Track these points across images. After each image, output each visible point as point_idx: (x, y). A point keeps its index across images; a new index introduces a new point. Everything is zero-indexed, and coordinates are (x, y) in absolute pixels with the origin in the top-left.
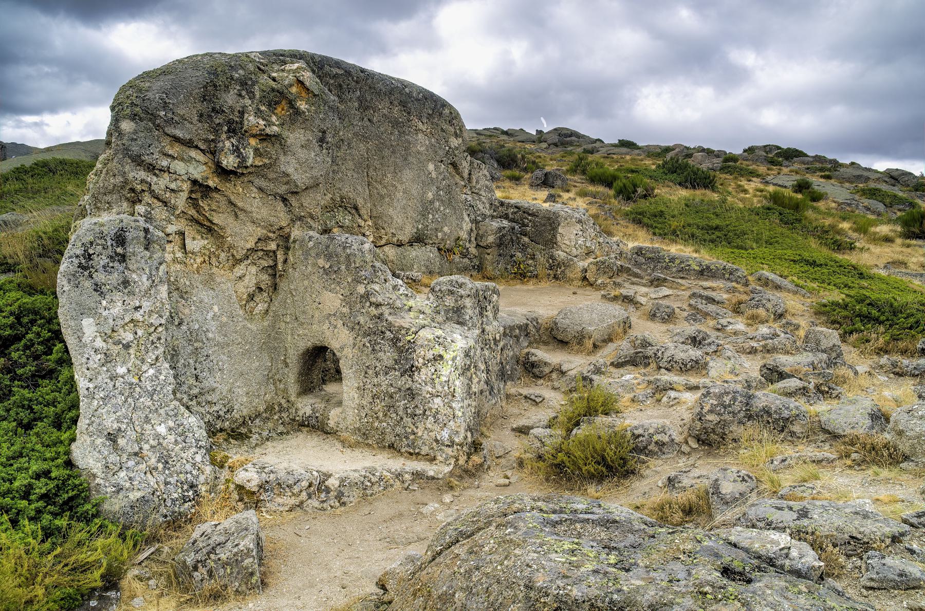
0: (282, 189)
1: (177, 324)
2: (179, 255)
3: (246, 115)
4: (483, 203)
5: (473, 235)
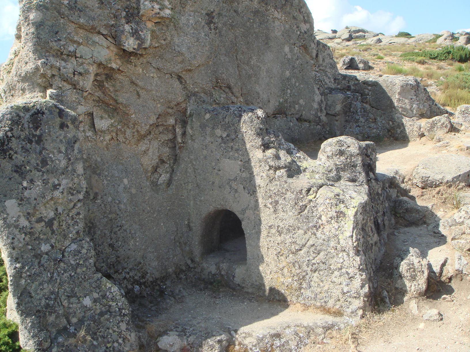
0: (177, 68)
1: (92, 198)
2: (90, 134)
4: (329, 78)
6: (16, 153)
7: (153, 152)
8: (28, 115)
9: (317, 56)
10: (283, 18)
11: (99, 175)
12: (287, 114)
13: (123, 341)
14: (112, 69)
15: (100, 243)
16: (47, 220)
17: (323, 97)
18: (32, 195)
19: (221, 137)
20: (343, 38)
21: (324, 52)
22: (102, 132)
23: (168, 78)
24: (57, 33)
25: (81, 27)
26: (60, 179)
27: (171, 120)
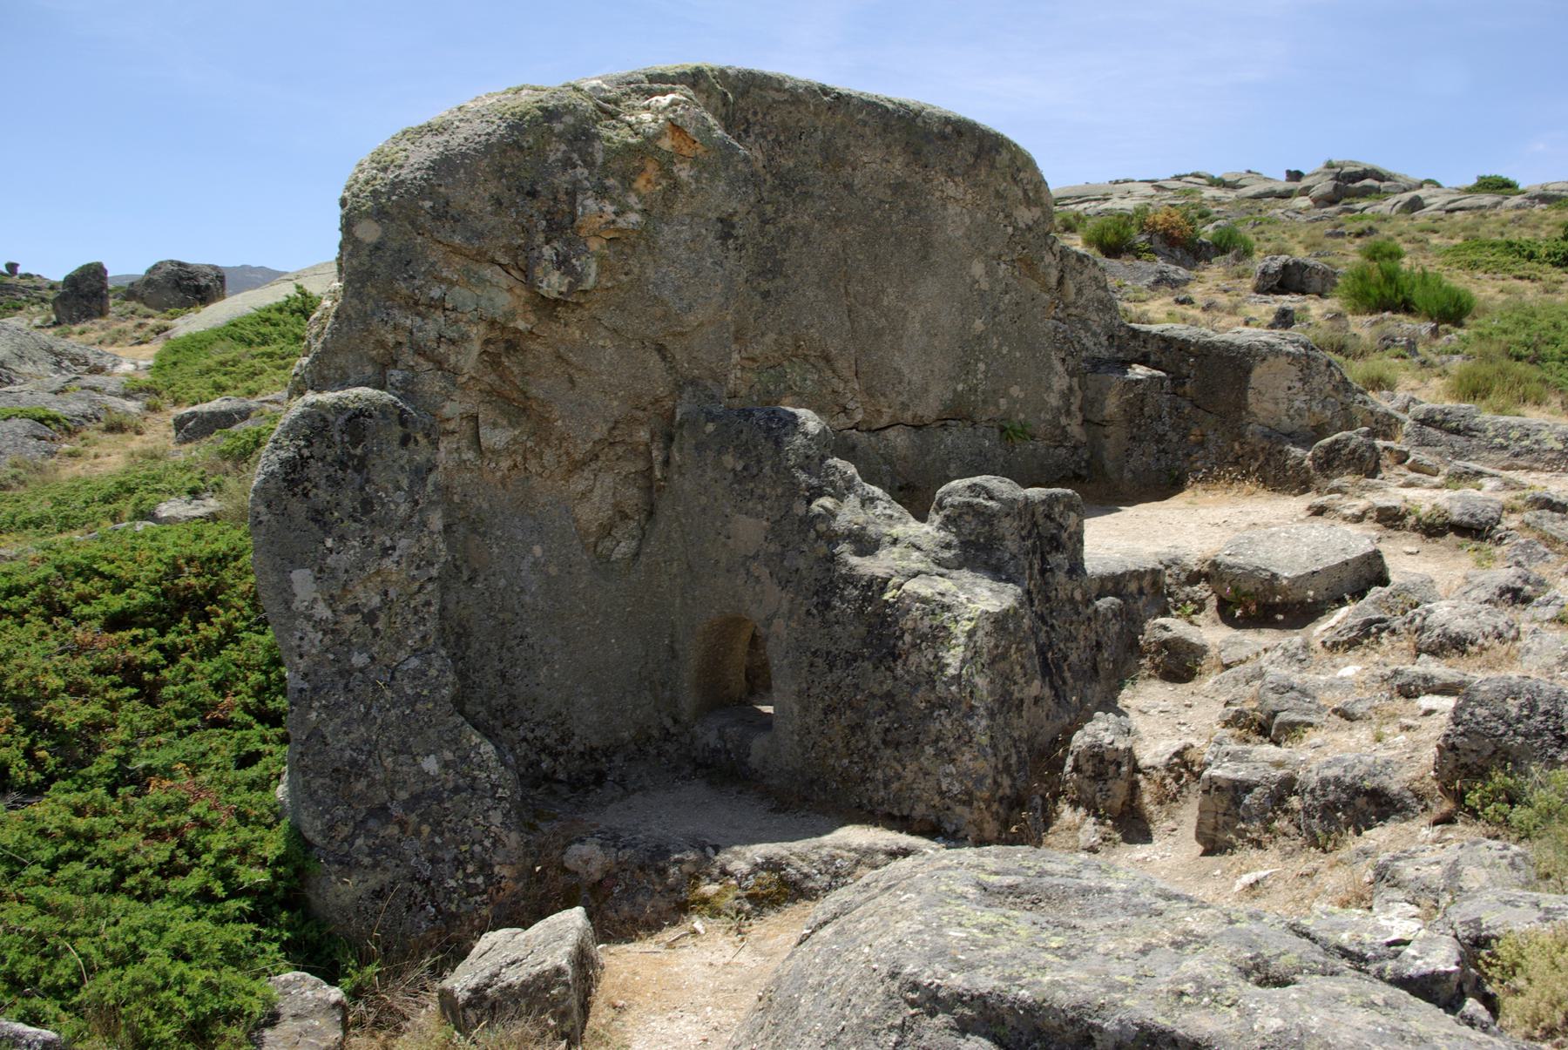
1: (465, 578)
2: (469, 455)
3: (580, 197)
4: (1095, 334)
5: (1076, 402)
6: (315, 486)
7: (602, 496)
8: (341, 420)
9: (1061, 281)
10: (969, 197)
11: (484, 535)
12: (977, 419)
13: (494, 844)
14: (516, 331)
15: (477, 667)
16: (366, 611)
17: (1075, 380)
18: (342, 563)
19: (733, 470)
20: (1315, 193)
21: (1081, 273)
22: (494, 452)
23: (636, 349)
24: (408, 263)
25: (456, 251)
26: (396, 538)
27: (642, 433)
